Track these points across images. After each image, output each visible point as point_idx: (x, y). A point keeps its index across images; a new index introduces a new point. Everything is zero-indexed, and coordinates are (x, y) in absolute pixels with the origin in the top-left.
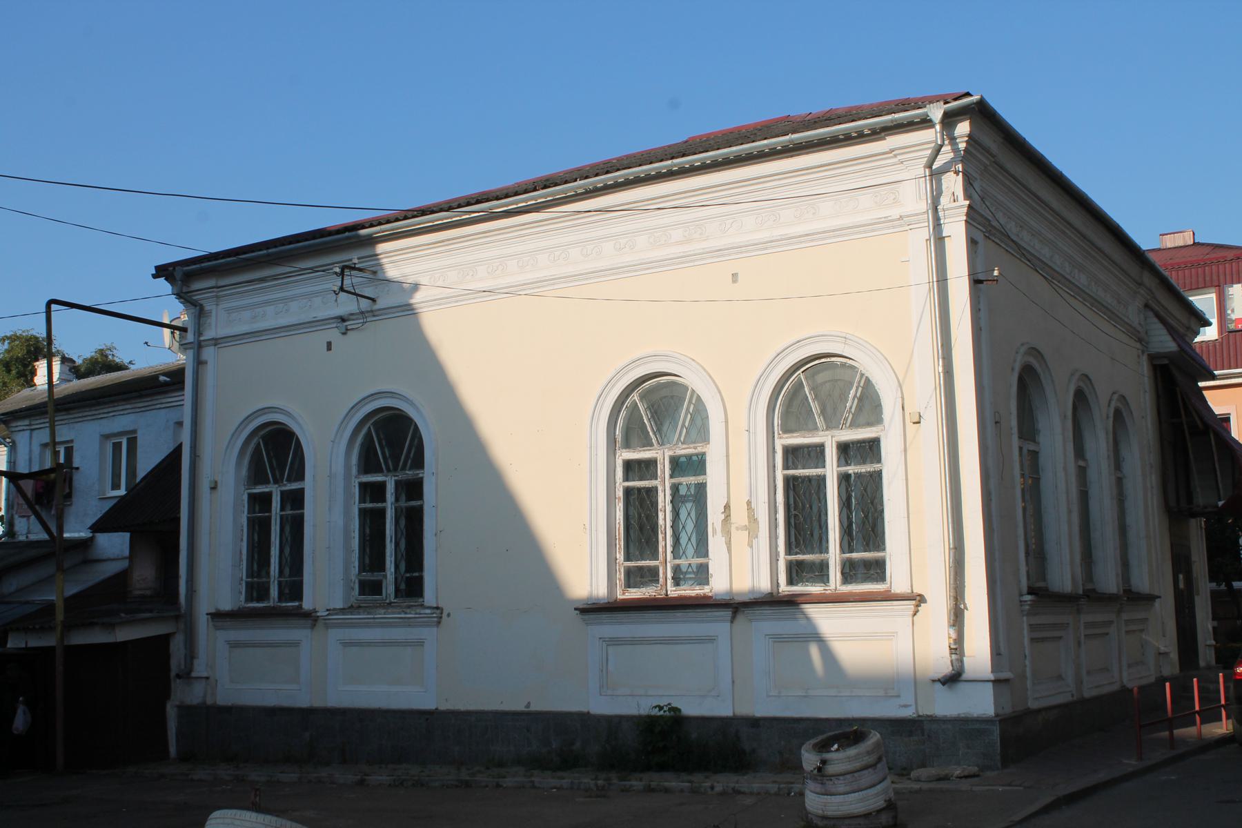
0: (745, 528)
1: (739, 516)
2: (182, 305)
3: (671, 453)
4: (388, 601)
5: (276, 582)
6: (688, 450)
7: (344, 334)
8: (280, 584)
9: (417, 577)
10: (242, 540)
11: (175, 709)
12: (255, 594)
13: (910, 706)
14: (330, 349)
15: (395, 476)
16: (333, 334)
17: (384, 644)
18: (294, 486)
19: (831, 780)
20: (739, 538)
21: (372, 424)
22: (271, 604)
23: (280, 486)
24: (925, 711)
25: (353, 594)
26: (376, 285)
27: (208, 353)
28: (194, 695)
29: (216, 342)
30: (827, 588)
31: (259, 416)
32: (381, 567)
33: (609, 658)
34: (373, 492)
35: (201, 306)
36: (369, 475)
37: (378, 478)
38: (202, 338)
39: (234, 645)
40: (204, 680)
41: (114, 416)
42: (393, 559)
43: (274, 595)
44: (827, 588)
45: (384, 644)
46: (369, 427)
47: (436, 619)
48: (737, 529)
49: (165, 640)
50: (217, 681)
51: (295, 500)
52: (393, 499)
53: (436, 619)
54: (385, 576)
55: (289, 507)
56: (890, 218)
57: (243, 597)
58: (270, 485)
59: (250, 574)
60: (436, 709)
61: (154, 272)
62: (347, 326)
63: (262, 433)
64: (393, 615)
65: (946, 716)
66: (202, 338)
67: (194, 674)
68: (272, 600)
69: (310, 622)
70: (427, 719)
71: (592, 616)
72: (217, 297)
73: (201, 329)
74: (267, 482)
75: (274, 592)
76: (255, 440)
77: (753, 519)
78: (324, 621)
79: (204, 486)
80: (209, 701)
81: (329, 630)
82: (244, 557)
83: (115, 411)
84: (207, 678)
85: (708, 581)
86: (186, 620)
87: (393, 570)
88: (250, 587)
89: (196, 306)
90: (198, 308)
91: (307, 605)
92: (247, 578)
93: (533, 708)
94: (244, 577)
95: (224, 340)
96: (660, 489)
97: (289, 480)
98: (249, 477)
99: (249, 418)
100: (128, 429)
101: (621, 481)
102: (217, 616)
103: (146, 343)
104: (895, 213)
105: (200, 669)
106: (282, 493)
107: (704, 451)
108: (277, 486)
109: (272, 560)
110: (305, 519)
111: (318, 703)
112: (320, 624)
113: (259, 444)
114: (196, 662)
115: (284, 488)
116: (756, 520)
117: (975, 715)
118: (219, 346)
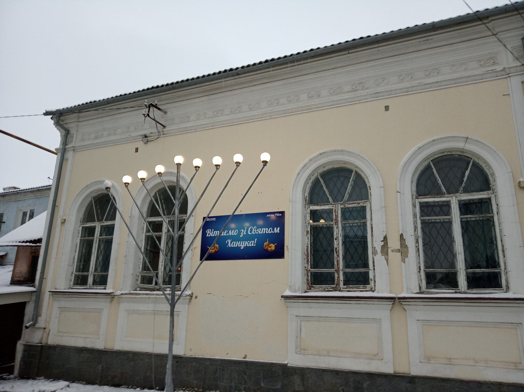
0: (399, 251)
1: (394, 243)
3: (342, 206)
5: (92, 275)
7: (146, 143)
8: (94, 276)
10: (76, 251)
12: (79, 282)
14: (137, 152)
16: (140, 144)
18: (109, 223)
20: (395, 257)
23: (100, 223)
25: (137, 283)
27: (69, 155)
33: (302, 329)
37: (158, 219)
42: (163, 264)
43: (90, 282)
46: (156, 193)
48: (393, 251)
50: (50, 331)
51: (109, 230)
55: (104, 234)
56: (495, 70)
58: (95, 222)
59: (78, 269)
62: (148, 139)
66: (67, 147)
68: (88, 285)
70: (177, 362)
74: (94, 221)
80: (522, 46)
84: (45, 328)
85: (369, 283)
86: (38, 295)
87: (163, 270)
88: (77, 278)
90: (67, 131)
92: (76, 272)
96: (335, 227)
97: (106, 220)
98: (84, 218)
102: (54, 293)
103: (49, 178)
105: (41, 323)
106: (102, 227)
107: (364, 205)
108: (99, 223)
113: (92, 200)
114: (40, 319)
115: (103, 224)
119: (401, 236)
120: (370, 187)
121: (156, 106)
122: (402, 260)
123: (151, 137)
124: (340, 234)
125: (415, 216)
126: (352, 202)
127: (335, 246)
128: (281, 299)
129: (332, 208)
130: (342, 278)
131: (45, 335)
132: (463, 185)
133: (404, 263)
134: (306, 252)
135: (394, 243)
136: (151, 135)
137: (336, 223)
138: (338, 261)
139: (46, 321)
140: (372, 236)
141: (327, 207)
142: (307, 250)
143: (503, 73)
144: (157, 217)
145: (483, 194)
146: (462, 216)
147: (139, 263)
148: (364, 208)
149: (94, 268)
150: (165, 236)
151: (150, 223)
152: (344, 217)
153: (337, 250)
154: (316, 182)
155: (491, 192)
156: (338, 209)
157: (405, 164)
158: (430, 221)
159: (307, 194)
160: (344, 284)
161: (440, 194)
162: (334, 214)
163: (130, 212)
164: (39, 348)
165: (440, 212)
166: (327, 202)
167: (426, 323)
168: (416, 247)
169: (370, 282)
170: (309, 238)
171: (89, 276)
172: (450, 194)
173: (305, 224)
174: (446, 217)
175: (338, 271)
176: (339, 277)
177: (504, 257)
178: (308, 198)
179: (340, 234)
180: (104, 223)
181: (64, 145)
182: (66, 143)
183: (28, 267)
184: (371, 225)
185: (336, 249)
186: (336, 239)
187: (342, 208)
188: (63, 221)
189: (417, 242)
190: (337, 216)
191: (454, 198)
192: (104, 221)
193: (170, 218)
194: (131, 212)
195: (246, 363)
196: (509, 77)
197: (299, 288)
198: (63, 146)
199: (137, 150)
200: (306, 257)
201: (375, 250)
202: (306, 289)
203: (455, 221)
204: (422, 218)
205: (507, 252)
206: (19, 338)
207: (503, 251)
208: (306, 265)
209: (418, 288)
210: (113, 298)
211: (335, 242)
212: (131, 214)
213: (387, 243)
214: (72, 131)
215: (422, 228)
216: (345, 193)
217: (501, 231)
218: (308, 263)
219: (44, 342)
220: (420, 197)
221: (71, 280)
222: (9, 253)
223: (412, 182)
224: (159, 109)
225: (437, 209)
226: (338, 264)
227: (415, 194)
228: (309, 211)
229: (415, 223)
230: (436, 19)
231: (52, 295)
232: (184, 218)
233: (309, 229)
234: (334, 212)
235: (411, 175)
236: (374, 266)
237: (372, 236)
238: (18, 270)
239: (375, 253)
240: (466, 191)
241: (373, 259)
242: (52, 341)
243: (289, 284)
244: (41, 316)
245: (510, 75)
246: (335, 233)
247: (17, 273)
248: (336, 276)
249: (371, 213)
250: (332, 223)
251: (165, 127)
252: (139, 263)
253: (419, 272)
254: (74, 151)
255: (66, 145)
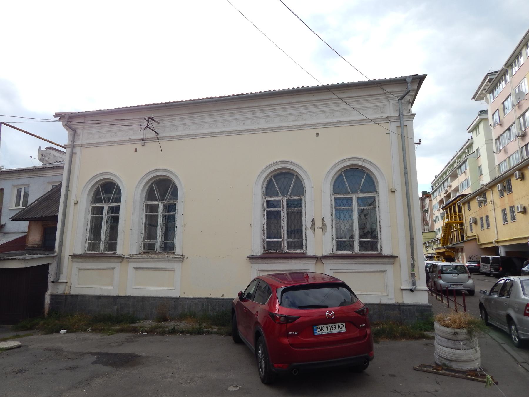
0: (321, 228)
1: (318, 223)
2: (66, 130)
3: (287, 198)
4: (157, 252)
5: (103, 243)
6: (295, 198)
9: (166, 242)
10: (88, 225)
11: (50, 296)
13: (393, 299)
14: (136, 151)
15: (163, 202)
16: (138, 146)
17: (156, 269)
19: (459, 342)
20: (318, 232)
21: (153, 182)
22: (100, 252)
24: (400, 301)
26: (159, 128)
27: (77, 150)
28: (61, 290)
29: (81, 145)
30: (353, 252)
31: (100, 176)
32: (155, 238)
34: (152, 209)
35: (75, 131)
36: (151, 202)
38: (75, 143)
39: (80, 269)
40: (65, 284)
41: (19, 178)
44: (353, 252)
45: (156, 269)
46: (152, 183)
47: (181, 260)
49: (47, 266)
51: (116, 210)
52: (162, 212)
53: (181, 260)
54: (157, 242)
56: (383, 117)
57: (86, 249)
58: (103, 204)
60: (180, 297)
61: (54, 115)
63: (101, 183)
64: (160, 257)
65: (408, 304)
66: (75, 143)
67: (60, 281)
69: (120, 260)
71: (254, 260)
72: (83, 128)
73: (75, 140)
75: (102, 247)
76: (97, 186)
77: (324, 225)
78: (127, 260)
79: (71, 202)
81: (129, 263)
82: (88, 233)
83: (20, 176)
85: (303, 248)
86: (59, 258)
89: (73, 130)
90: (74, 131)
91: (119, 252)
93: (225, 297)
94: (87, 241)
95: (85, 145)
97: (112, 202)
99: (95, 176)
100: (25, 183)
101: (265, 208)
102: (74, 257)
103: (31, 157)
104: (385, 116)
105: (63, 279)
107: (301, 198)
109: (102, 234)
110: (120, 218)
111: (122, 294)
112: (125, 260)
113: (99, 187)
114: (61, 276)
116: (325, 225)
117: (420, 303)
118: (83, 147)
119: (323, 219)
120: (305, 186)
121: (152, 119)
122: (323, 234)
123: (148, 141)
124: (285, 217)
125: (331, 206)
126: (293, 196)
127: (282, 225)
128: (247, 258)
129: (280, 199)
130: (286, 245)
131: (67, 288)
132: (360, 188)
133: (324, 235)
134: (263, 228)
135: (318, 223)
136: (147, 139)
137: (283, 210)
138: (283, 234)
139: (67, 277)
140: (305, 218)
141: (277, 199)
142: (264, 227)
143: (387, 119)
144: (154, 201)
145: (371, 194)
146: (359, 207)
147: (141, 235)
148: (301, 200)
149: (104, 238)
150: (161, 215)
151: (336, 199)
152: (288, 206)
153: (283, 227)
154: (270, 181)
155: (375, 193)
156: (284, 200)
157: (327, 174)
158: (340, 209)
159: (264, 189)
160: (287, 249)
161: (347, 193)
162: (282, 203)
163: (133, 197)
164: (64, 297)
165: (346, 203)
166: (277, 195)
167: (137, 269)
168: (332, 225)
169: (303, 247)
170: (265, 219)
171: (101, 243)
172: (352, 193)
173: (263, 210)
174: (350, 208)
175: (283, 241)
176: (284, 244)
177: (381, 232)
178: (264, 191)
179: (285, 217)
180: (110, 204)
181: (73, 142)
182: (74, 140)
183: (41, 236)
184: (305, 211)
185: (283, 226)
186: (283, 220)
187: (287, 200)
188: (76, 203)
189: (332, 222)
190: (283, 205)
191: (355, 196)
192: (110, 203)
193: (164, 202)
194: (134, 197)
195: (223, 299)
196: (390, 122)
197: (259, 252)
198: (72, 143)
199: (136, 150)
200: (263, 232)
201: (307, 227)
202: (263, 252)
203: (354, 211)
204: (336, 208)
205: (382, 230)
206: (46, 291)
207: (380, 229)
208: (263, 237)
209: (332, 251)
210: (123, 259)
211: (282, 222)
212: (134, 198)
213: (314, 223)
214: (79, 131)
215: (335, 214)
216: (289, 189)
217: (380, 217)
218: (264, 235)
219: (67, 292)
220: (335, 194)
221: (85, 247)
222: (7, 223)
223: (331, 185)
224: (154, 121)
225: (345, 202)
226: (284, 236)
227: (332, 192)
228: (265, 201)
229: (332, 211)
230: (351, 81)
231: (71, 258)
232: (175, 202)
233: (265, 213)
234: (282, 202)
235: (330, 180)
236: (306, 237)
237: (305, 218)
238: (32, 239)
239: (307, 229)
240: (362, 192)
241: (306, 233)
242: (73, 292)
243: (252, 249)
244: (62, 274)
245: (390, 121)
246: (282, 216)
247: (31, 241)
248: (282, 243)
249: (305, 204)
250: (280, 209)
251: (158, 134)
252: (141, 235)
253: (333, 241)
254: (82, 147)
255: (74, 142)
